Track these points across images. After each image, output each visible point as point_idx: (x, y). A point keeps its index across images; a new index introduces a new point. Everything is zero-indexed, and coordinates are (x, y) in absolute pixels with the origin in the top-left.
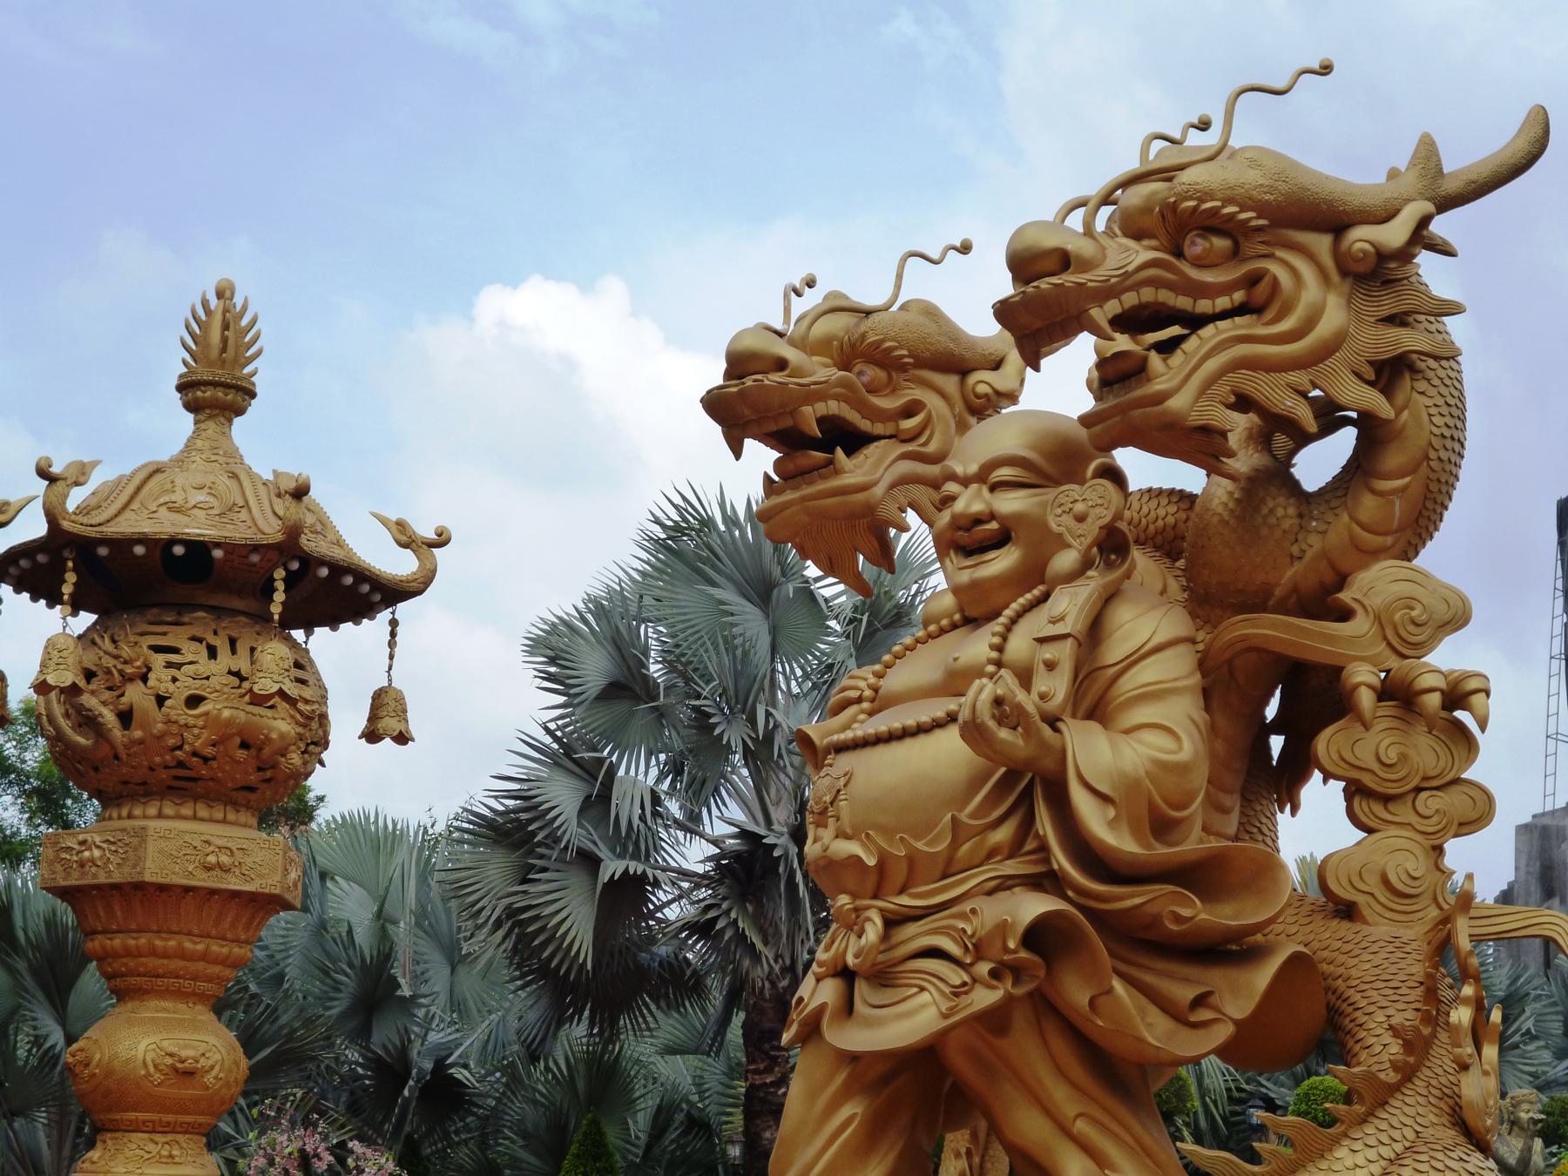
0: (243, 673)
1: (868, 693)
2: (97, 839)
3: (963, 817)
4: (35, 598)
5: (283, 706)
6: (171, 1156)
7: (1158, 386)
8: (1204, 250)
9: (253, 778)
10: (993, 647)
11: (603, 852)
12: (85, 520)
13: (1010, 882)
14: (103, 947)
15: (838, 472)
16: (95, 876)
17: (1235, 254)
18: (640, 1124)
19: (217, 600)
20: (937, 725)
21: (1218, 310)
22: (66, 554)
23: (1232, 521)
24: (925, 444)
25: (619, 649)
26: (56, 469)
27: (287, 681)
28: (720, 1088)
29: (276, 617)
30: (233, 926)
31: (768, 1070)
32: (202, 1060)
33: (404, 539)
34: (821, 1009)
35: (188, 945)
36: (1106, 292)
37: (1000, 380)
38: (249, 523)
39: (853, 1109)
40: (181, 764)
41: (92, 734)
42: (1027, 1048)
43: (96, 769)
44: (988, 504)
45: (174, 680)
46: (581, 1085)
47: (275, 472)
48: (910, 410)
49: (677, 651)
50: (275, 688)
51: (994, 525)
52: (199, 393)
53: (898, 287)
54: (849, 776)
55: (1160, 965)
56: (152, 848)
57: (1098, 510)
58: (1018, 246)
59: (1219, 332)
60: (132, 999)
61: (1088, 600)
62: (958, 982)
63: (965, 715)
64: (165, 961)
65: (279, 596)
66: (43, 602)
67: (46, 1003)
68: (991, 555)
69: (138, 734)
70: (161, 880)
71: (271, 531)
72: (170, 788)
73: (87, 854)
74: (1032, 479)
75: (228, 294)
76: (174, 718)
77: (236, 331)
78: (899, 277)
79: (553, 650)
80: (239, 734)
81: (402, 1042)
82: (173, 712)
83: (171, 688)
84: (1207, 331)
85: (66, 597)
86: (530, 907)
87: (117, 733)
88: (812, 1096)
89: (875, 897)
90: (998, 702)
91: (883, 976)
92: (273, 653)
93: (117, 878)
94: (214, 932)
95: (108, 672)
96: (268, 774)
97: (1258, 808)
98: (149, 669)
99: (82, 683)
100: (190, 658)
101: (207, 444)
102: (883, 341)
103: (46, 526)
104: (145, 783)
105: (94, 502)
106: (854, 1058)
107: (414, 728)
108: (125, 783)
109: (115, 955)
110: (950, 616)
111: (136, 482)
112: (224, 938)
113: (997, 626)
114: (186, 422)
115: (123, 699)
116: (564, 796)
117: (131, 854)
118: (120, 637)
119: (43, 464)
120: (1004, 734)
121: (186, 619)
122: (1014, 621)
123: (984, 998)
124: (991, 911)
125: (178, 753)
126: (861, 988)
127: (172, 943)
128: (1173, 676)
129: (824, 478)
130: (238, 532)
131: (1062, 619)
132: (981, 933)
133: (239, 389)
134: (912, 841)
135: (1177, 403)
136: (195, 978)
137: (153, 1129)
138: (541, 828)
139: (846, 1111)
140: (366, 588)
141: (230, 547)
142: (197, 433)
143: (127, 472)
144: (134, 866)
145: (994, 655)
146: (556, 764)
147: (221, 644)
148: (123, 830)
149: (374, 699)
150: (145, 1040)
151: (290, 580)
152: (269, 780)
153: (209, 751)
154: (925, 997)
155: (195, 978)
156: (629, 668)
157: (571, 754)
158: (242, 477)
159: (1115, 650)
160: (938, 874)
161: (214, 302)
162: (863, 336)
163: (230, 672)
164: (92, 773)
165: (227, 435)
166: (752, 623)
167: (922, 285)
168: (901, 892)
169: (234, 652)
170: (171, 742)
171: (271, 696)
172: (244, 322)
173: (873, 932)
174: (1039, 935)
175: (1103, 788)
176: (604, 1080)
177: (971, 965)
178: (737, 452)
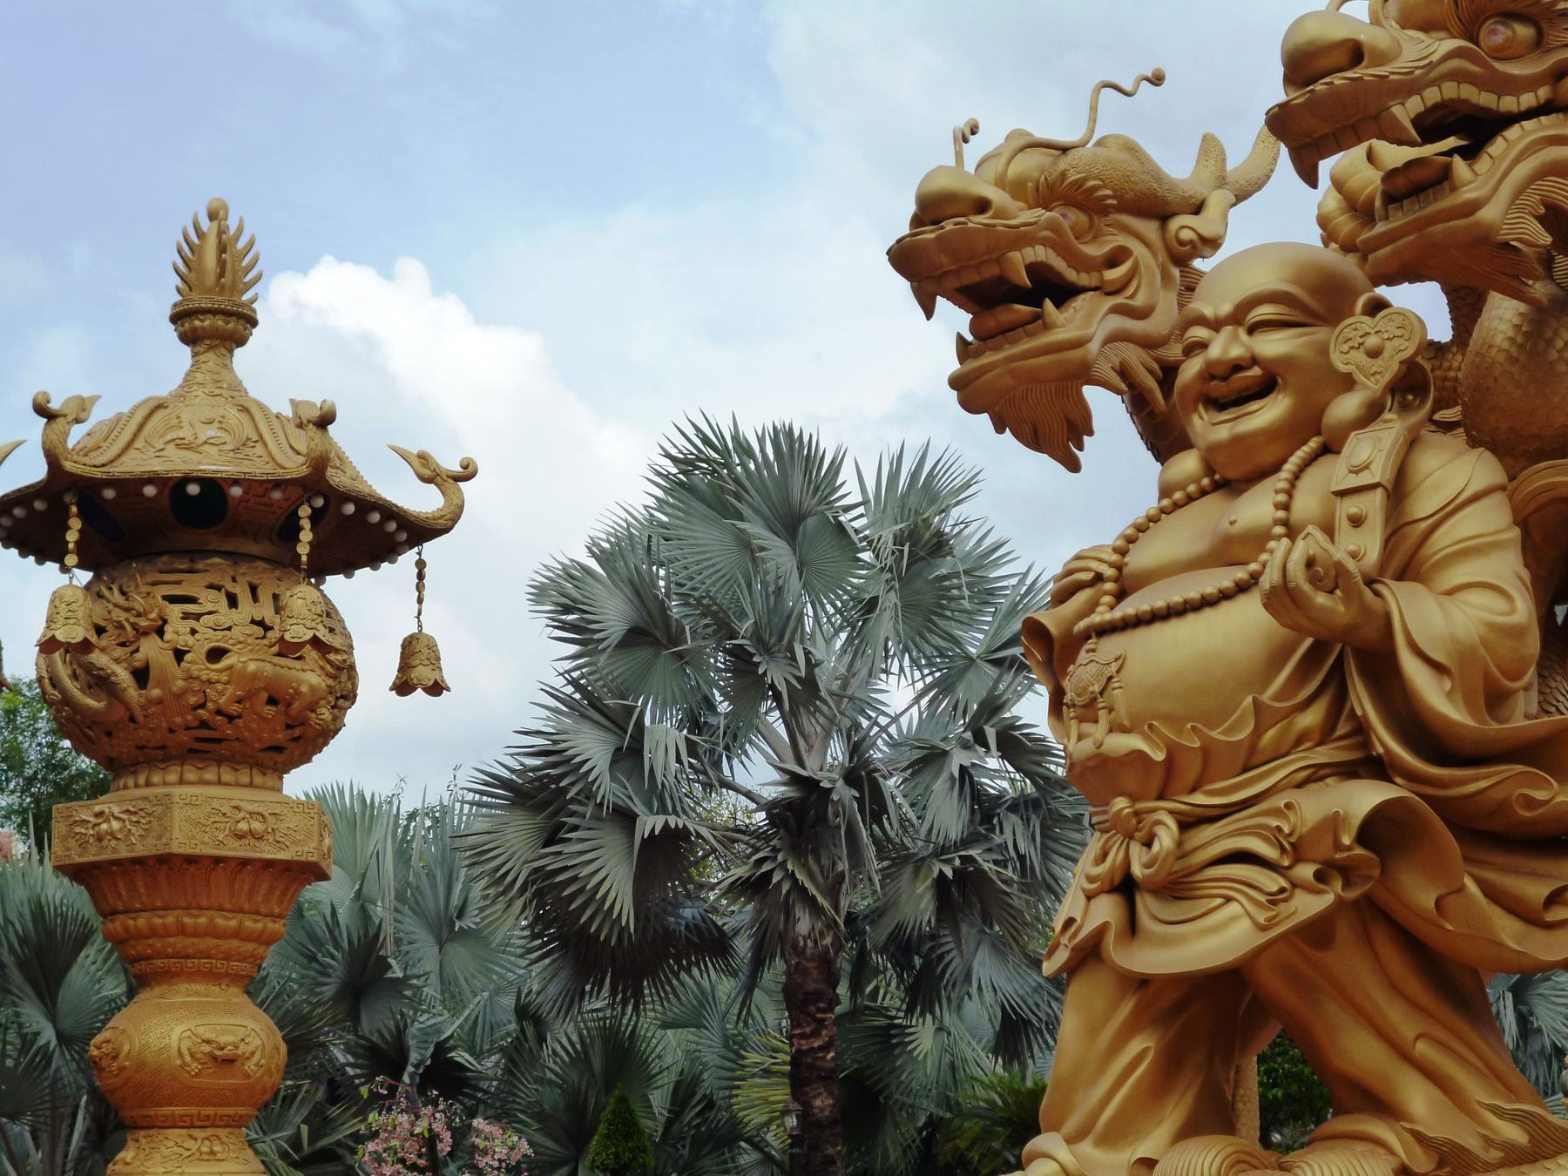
0: (267, 622)
1: (1109, 572)
2: (116, 810)
3: (1266, 697)
4: (23, 554)
5: (311, 654)
6: (212, 1153)
7: (1468, 194)
8: (1507, 40)
9: (281, 737)
10: (1278, 506)
11: (638, 808)
12: (87, 460)
13: (1322, 772)
14: (126, 929)
15: (1048, 327)
16: (115, 850)
17: (1540, 44)
18: (659, 1099)
19: (229, 546)
20: (1225, 596)
21: (1523, 107)
22: (68, 498)
23: (1522, 358)
24: (1132, 297)
25: (637, 593)
26: (54, 405)
27: (320, 627)
28: (719, 1061)
29: (304, 558)
30: (267, 899)
31: (815, 1034)
32: (242, 1046)
33: (427, 473)
34: (1101, 931)
35: (220, 921)
36: (1410, 87)
37: (1201, 224)
38: (266, 458)
39: (1143, 1044)
40: (203, 724)
41: (103, 695)
42: (1348, 960)
43: (109, 734)
44: (1248, 348)
45: (193, 632)
46: (597, 1062)
47: (292, 401)
48: (1114, 260)
49: (696, 594)
50: (309, 635)
51: (1256, 371)
52: (197, 323)
53: (1093, 120)
54: (1121, 661)
55: (1500, 859)
56: (178, 815)
57: (1396, 342)
58: (925, 189)
59: (1525, 133)
60: (160, 983)
61: (1394, 445)
62: (1274, 889)
63: (1270, 578)
64: (195, 940)
65: (306, 536)
66: (32, 558)
67: (38, 1002)
68: (1254, 406)
69: (156, 692)
70: (189, 851)
71: (295, 466)
72: (191, 751)
73: (104, 826)
74: (1300, 318)
75: (222, 214)
76: (195, 674)
77: (232, 256)
78: (1094, 109)
79: (565, 600)
80: (265, 689)
81: (398, 1028)
82: (193, 668)
83: (191, 640)
84: (1513, 132)
85: (71, 546)
86: (566, 868)
87: (133, 693)
88: (1092, 1031)
89: (1160, 797)
90: (1310, 563)
91: (1177, 886)
92: (300, 596)
93: (141, 850)
94: (247, 907)
95: (120, 626)
96: (297, 732)
97: (1553, 684)
98: (165, 622)
99: (93, 638)
100: (209, 607)
101: (208, 377)
102: (1085, 179)
103: (45, 468)
104: (163, 747)
105: (91, 443)
106: (1143, 983)
107: (449, 676)
108: (142, 748)
109: (139, 936)
110: (1198, 481)
111: (138, 419)
112: (258, 913)
113: (1281, 479)
115: (138, 656)
116: (593, 748)
117: (155, 824)
118: (130, 589)
119: (41, 400)
120: (1321, 599)
121: (200, 566)
122: (1297, 476)
123: (1308, 906)
124: (1313, 806)
125: (201, 711)
126: (1147, 905)
127: (202, 920)
128: (1492, 527)
129: (1030, 335)
130: (257, 467)
131: (1367, 467)
132: (1302, 830)
133: (240, 316)
134: (1205, 730)
135: (1489, 214)
136: (227, 957)
137: (190, 1124)
138: (572, 784)
139: (1136, 1046)
140: (392, 526)
141: (247, 483)
142: (196, 366)
143: (126, 409)
144: (160, 838)
145: (1281, 514)
146: (583, 716)
148: (145, 798)
149: (403, 647)
150: (172, 1028)
151: (315, 518)
152: (296, 739)
153: (234, 709)
154: (1233, 908)
155: (227, 958)
156: (648, 612)
157: (592, 703)
158: (254, 410)
159: (1423, 505)
160: (1240, 765)
161: (205, 224)
162: (1063, 175)
163: (253, 622)
164: (105, 739)
165: (227, 367)
166: (778, 554)
167: (1116, 118)
168: (1193, 790)
169: (255, 599)
170: (193, 700)
171: (301, 645)
172: (241, 245)
173: (1166, 838)
174: (1376, 829)
175: (1438, 656)
176: (620, 1058)
177: (1290, 868)
178: (929, 313)
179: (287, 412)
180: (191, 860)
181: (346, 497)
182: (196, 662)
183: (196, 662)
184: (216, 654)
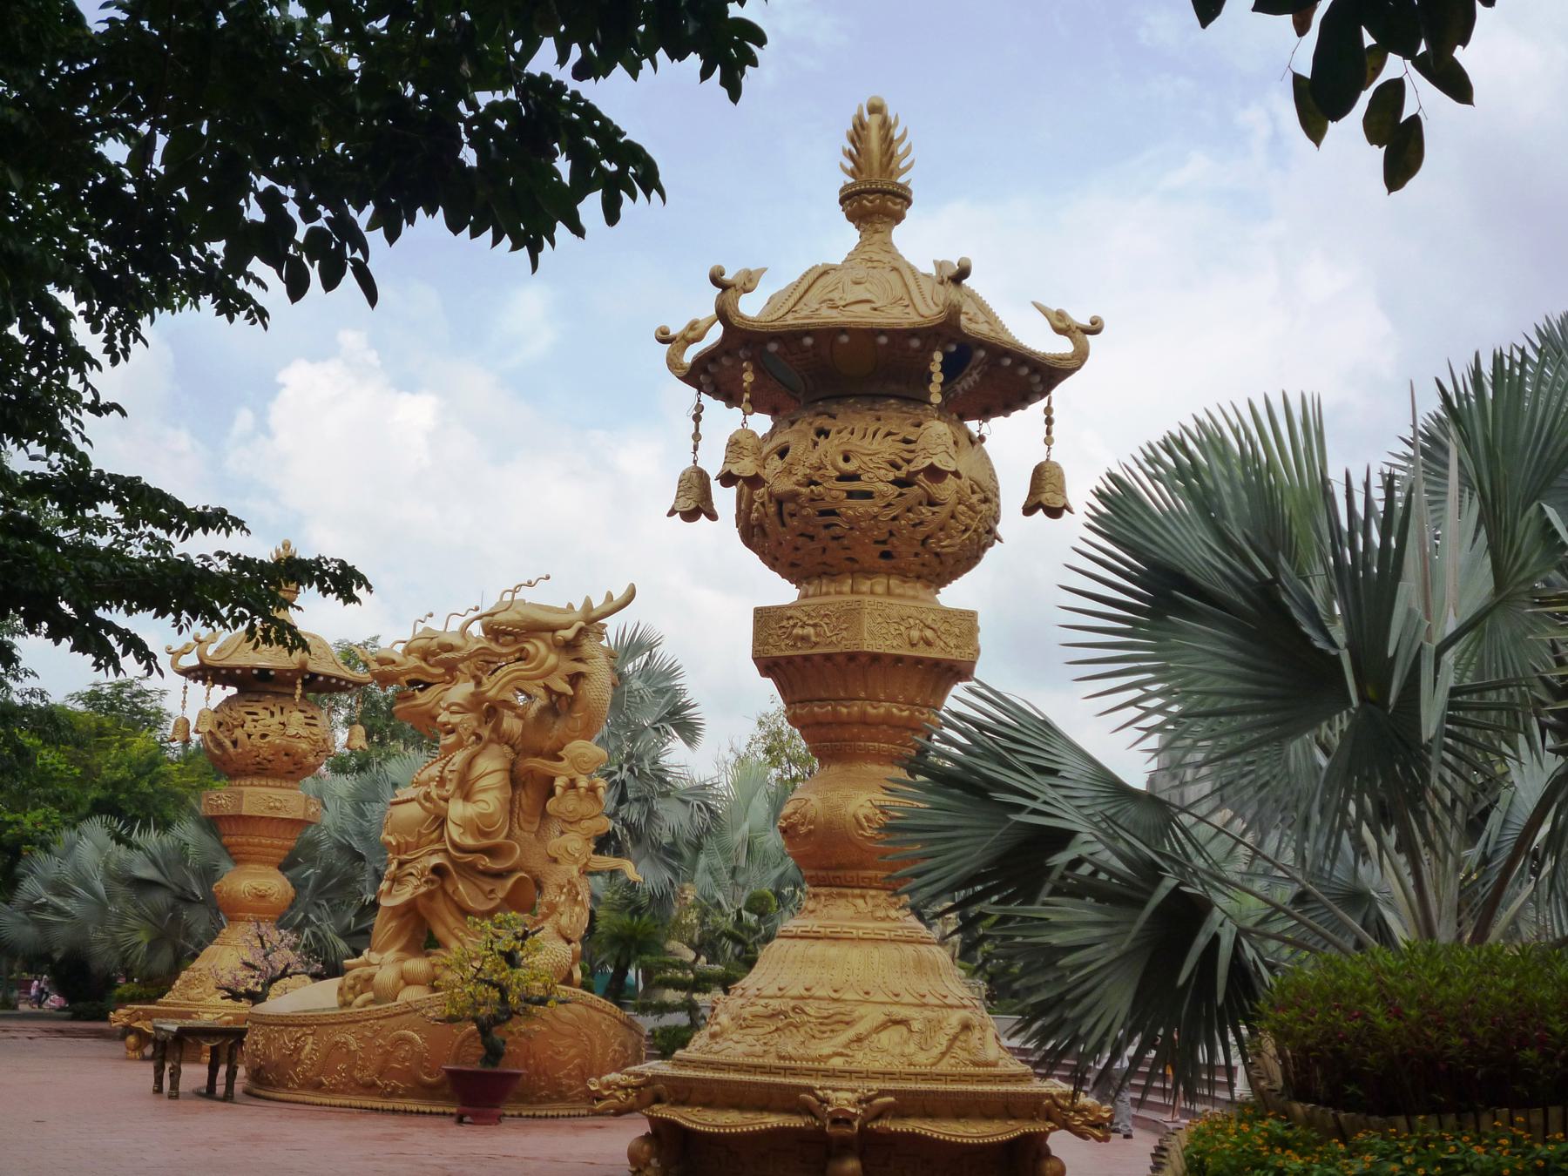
9: (292, 768)
14: (864, 713)
17: (516, 641)
26: (728, 276)
33: (1061, 325)
39: (393, 924)
87: (231, 749)
114: (850, 235)
147: (277, 710)
179: (932, 271)
180: (876, 658)
181: (982, 343)
182: (256, 739)
183: (256, 739)
184: (264, 736)
